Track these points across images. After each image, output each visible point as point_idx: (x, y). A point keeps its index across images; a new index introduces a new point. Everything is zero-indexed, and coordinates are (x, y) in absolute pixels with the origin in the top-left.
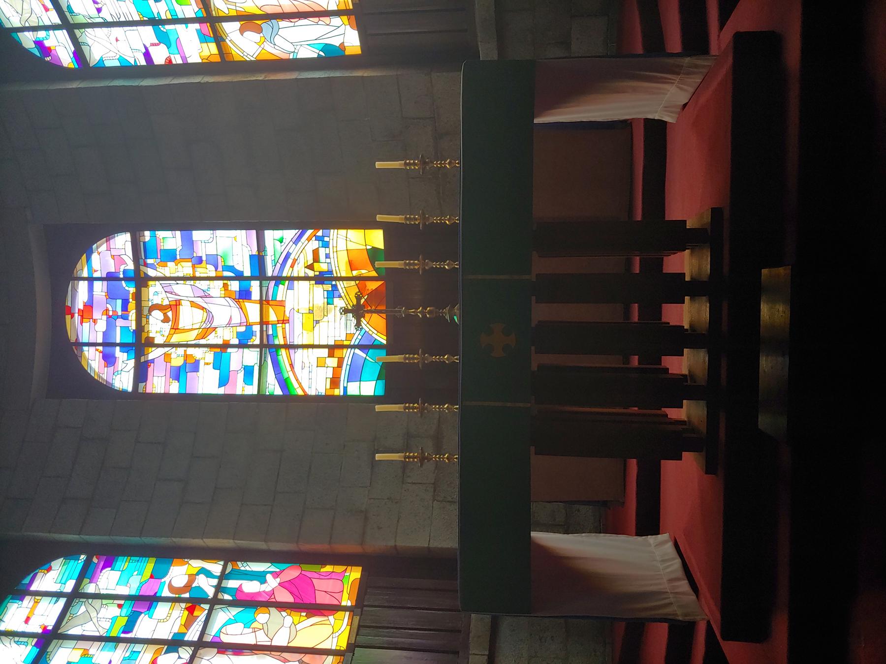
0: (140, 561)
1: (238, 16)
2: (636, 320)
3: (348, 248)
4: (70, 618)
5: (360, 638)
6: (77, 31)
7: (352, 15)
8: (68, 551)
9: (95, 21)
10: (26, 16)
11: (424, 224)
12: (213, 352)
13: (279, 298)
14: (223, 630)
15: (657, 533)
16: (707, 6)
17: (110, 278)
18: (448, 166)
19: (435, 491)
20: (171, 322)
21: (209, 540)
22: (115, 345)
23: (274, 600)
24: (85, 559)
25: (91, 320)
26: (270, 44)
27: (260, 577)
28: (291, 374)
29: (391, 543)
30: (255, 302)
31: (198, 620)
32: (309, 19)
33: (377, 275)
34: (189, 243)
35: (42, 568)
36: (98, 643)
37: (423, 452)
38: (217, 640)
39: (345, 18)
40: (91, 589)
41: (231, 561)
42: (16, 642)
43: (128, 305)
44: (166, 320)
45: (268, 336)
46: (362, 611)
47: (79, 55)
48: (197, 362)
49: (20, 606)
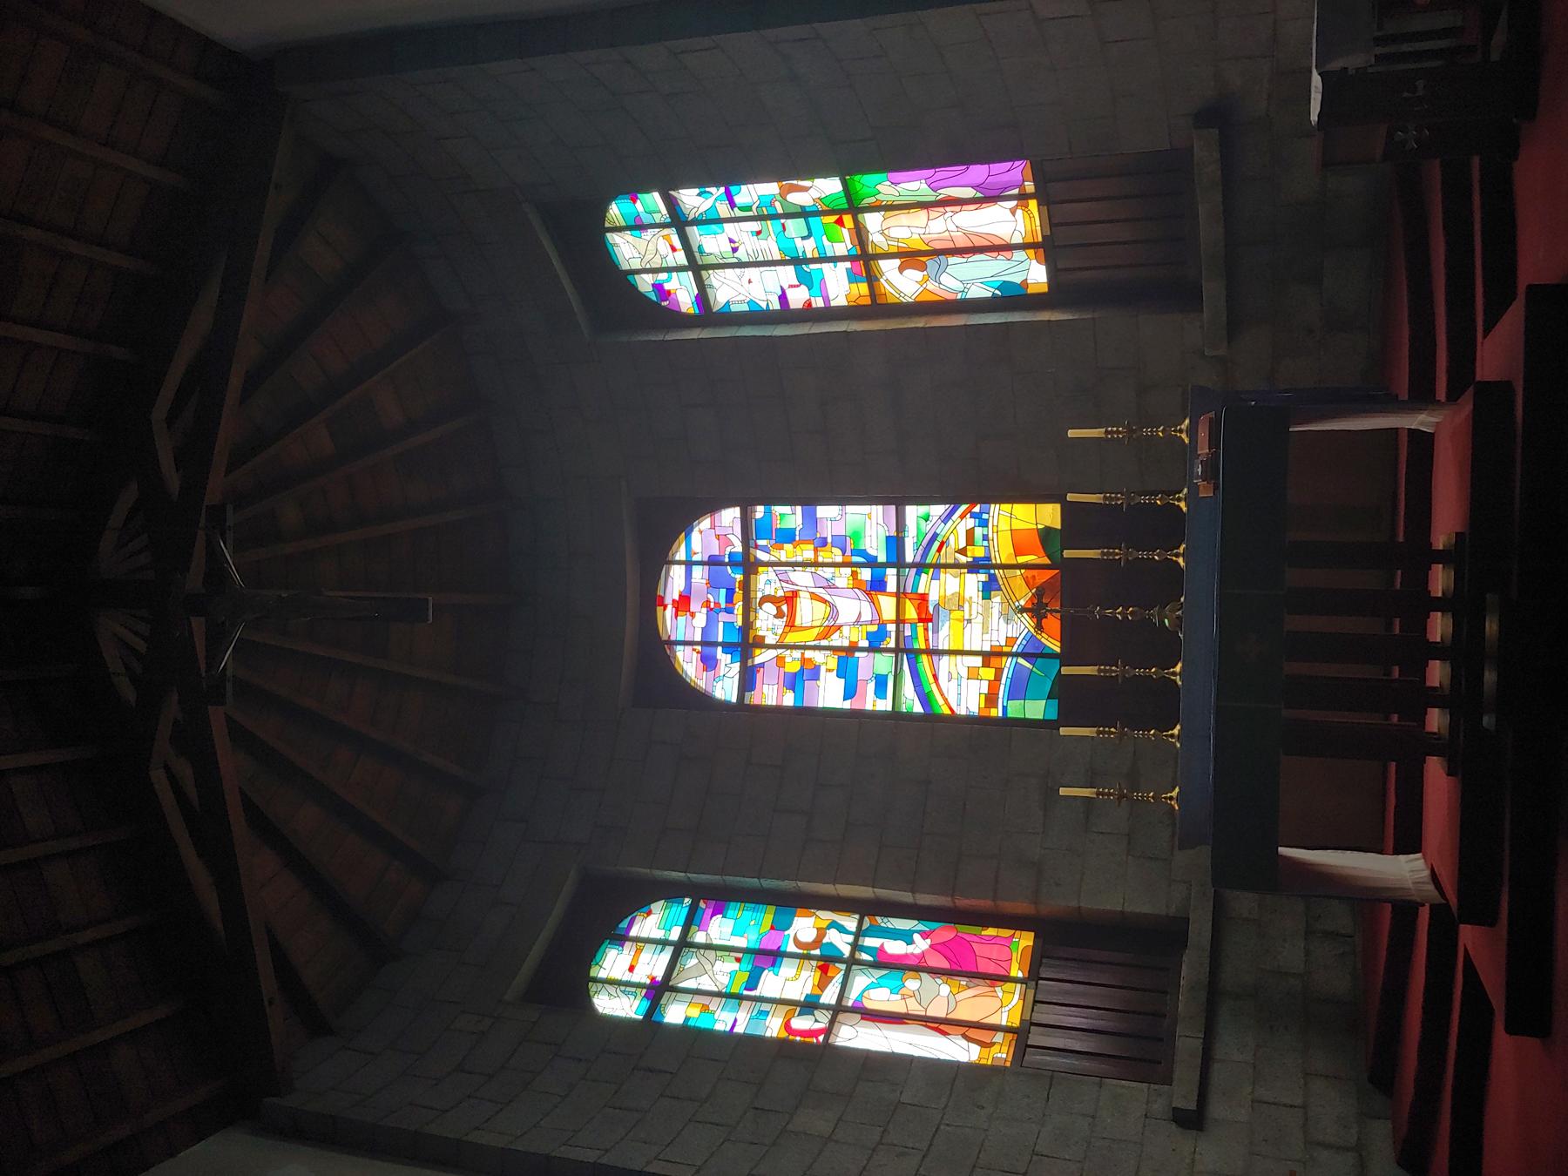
1: (899, 253)
2: (1398, 587)
3: (1013, 528)
6: (704, 273)
8: (671, 892)
10: (648, 257)
11: (1129, 505)
13: (921, 590)
14: (865, 994)
16: (1430, 588)
17: (713, 562)
19: (1129, 843)
20: (785, 618)
22: (716, 644)
23: (925, 964)
25: (688, 613)
26: (935, 283)
27: (907, 937)
28: (934, 686)
29: (1074, 904)
30: (890, 594)
33: (1050, 562)
34: (811, 521)
35: (641, 910)
39: (1031, 252)
40: (700, 937)
43: (733, 597)
44: (779, 615)
46: (1037, 984)
47: (702, 299)
48: (817, 669)
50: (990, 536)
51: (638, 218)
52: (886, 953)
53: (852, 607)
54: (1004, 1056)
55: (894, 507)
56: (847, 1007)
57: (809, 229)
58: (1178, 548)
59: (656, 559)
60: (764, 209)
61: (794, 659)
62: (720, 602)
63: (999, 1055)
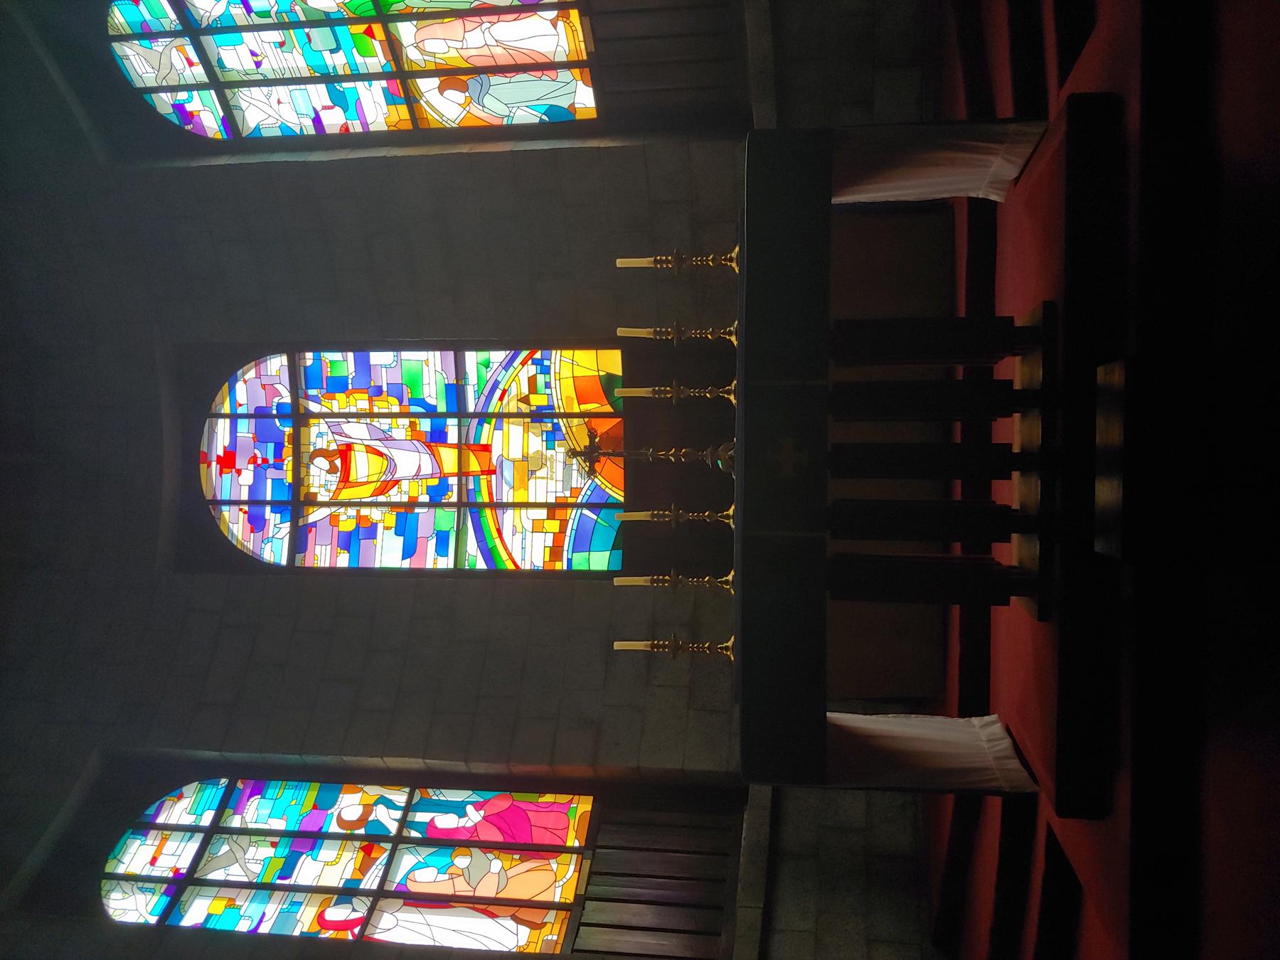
0: (299, 786)
3: (575, 375)
4: (209, 859)
5: (592, 889)
6: (228, 92)
7: (586, 67)
8: (205, 774)
9: (251, 79)
10: (164, 72)
12: (395, 513)
13: (483, 442)
14: (410, 876)
15: (988, 714)
17: (260, 414)
18: (711, 264)
21: (391, 759)
23: (477, 839)
24: (226, 783)
27: (459, 809)
28: (498, 541)
30: (452, 446)
31: (377, 863)
32: (530, 73)
33: (612, 411)
34: (364, 367)
35: (171, 794)
36: (247, 890)
37: (676, 641)
38: (403, 889)
39: (577, 71)
40: (236, 822)
41: (419, 787)
42: (140, 889)
44: (332, 470)
45: (468, 491)
46: (593, 855)
47: (229, 122)
49: (143, 843)
50: (553, 385)
51: (144, 24)
52: (437, 828)
53: (411, 461)
54: (555, 938)
55: (452, 353)
56: (390, 891)
57: (337, 40)
58: (730, 385)
59: (202, 412)
60: (284, 14)
61: (349, 517)
62: (268, 457)
63: (550, 937)
